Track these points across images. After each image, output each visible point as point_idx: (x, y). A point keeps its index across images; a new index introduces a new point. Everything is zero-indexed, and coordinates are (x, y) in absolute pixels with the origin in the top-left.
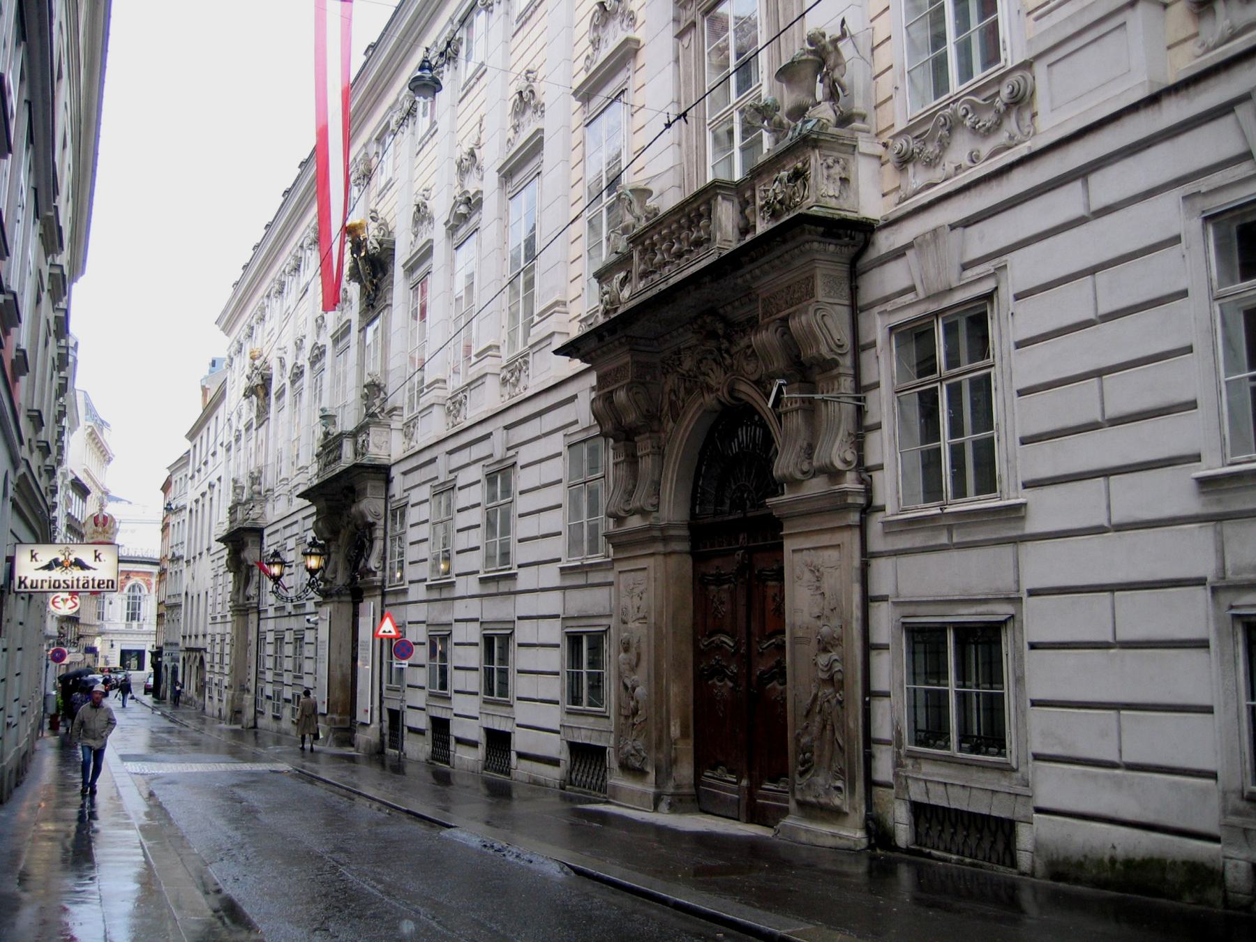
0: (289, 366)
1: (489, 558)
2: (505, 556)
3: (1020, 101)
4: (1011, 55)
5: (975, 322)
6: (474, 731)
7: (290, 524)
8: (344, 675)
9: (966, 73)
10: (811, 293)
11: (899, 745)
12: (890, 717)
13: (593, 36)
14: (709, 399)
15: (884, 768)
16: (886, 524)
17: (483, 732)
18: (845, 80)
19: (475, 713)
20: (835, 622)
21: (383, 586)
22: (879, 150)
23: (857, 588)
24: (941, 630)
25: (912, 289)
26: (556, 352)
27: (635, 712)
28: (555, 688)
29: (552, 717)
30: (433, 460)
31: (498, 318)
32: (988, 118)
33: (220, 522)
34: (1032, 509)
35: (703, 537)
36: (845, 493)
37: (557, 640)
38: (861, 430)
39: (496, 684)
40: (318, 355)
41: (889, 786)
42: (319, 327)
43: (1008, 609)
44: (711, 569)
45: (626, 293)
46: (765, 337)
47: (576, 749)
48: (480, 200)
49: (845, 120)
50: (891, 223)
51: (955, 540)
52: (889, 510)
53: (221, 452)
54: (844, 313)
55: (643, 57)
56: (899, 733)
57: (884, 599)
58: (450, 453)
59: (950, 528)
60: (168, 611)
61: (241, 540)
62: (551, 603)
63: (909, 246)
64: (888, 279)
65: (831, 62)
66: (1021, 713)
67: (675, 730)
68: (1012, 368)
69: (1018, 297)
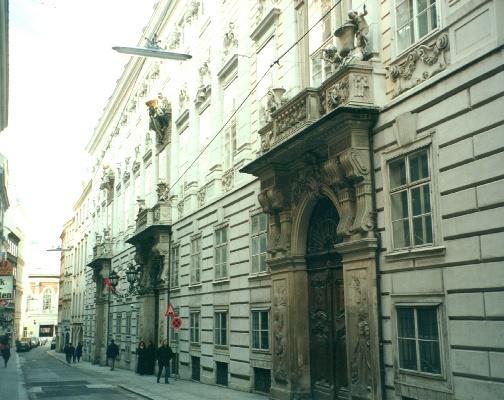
0: (123, 173)
1: (217, 272)
2: (225, 273)
3: (445, 48)
4: (442, 24)
5: (420, 158)
6: (211, 364)
7: (124, 256)
8: (151, 334)
9: (423, 32)
10: (350, 145)
11: (396, 368)
12: (392, 354)
13: (258, 5)
14: (310, 195)
15: (390, 379)
16: (387, 257)
17: (253, 371)
18: (367, 36)
19: (187, 350)
20: (366, 306)
21: (168, 289)
22: (385, 71)
23: (375, 289)
24: (411, 309)
25: (395, 142)
26: (241, 171)
27: (281, 352)
28: (246, 340)
29: (245, 354)
30: (190, 223)
31: (212, 160)
32: (431, 55)
33: (89, 255)
34: (448, 251)
35: (311, 262)
36: (367, 243)
37: (248, 315)
38: (375, 213)
39: (222, 338)
40: (137, 167)
41: (392, 388)
42: (137, 153)
43: (440, 300)
44: (315, 277)
45: (272, 142)
46: (330, 165)
47: (257, 371)
48: (210, 90)
49: (367, 57)
50: (387, 109)
51: (417, 266)
52: (388, 251)
53: (91, 217)
54: (366, 154)
55: (281, 17)
56: (396, 362)
57: (387, 294)
58: (199, 219)
59: (414, 260)
60: (64, 303)
61: (98, 265)
62: (244, 296)
63: (394, 121)
64: (385, 137)
65: (360, 27)
66: (446, 351)
67: (300, 360)
68: (440, 182)
69: (441, 147)
